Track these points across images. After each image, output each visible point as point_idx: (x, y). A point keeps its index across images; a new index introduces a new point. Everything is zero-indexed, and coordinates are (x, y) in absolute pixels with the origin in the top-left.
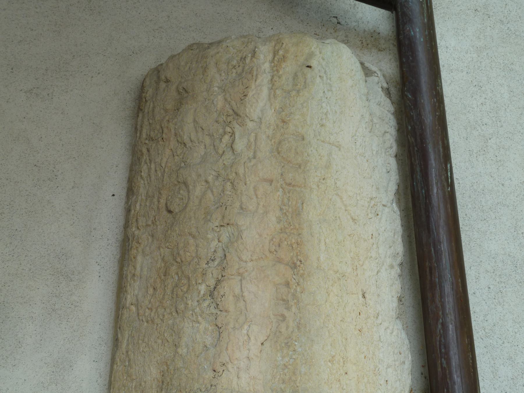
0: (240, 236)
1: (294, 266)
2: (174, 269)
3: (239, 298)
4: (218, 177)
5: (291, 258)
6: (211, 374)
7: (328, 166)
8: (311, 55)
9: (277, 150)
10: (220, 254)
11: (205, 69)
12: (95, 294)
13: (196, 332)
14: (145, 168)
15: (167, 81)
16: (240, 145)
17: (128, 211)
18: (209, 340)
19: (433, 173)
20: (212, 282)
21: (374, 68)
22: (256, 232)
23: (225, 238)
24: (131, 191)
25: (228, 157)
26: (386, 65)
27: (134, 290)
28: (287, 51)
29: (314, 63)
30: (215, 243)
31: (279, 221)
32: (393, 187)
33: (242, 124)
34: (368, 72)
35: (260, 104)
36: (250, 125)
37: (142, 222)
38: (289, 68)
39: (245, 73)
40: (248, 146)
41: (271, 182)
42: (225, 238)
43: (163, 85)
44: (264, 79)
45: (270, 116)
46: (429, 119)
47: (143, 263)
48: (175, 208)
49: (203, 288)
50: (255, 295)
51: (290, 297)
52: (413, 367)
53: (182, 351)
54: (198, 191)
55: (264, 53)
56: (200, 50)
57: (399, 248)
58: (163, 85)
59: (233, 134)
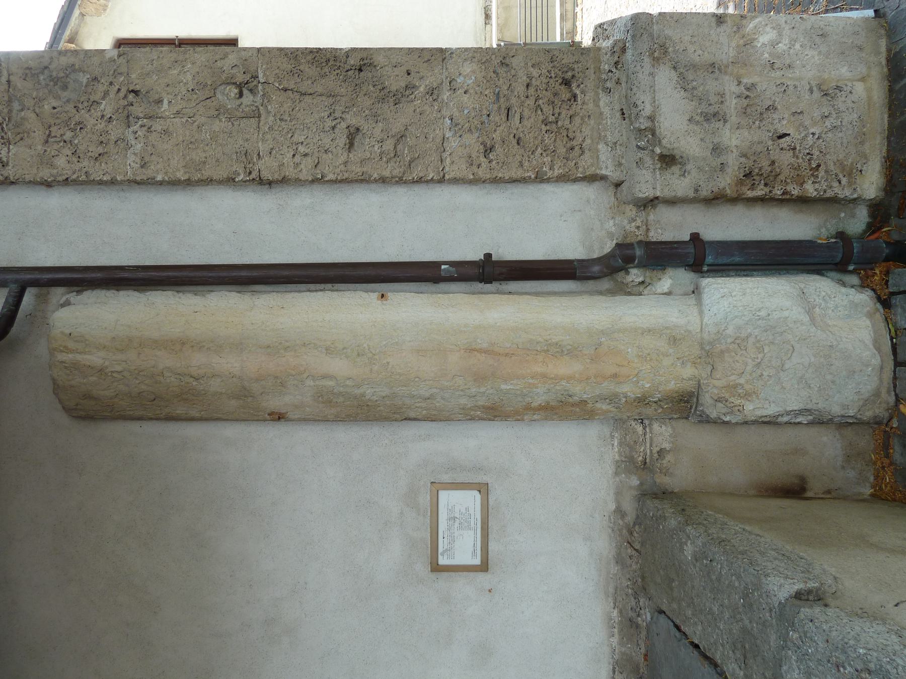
0: (169, 368)
1: (183, 344)
2: (184, 396)
3: (199, 367)
4: (136, 378)
5: (180, 344)
6: (234, 379)
7: (129, 327)
8: (62, 333)
9: (122, 351)
10: (177, 376)
11: (72, 386)
12: (192, 431)
13: (215, 385)
14: (128, 413)
15: (77, 405)
16: (119, 368)
17: (151, 419)
18: (219, 380)
19: (126, 275)
20: (192, 379)
21: (64, 299)
22: (165, 360)
23: (169, 374)
24: (140, 419)
25: (126, 374)
26: (58, 294)
27: (194, 413)
28: (61, 346)
29: (67, 332)
30: (172, 379)
31: (160, 350)
32: (136, 294)
33: (107, 367)
34: (67, 303)
35: (95, 359)
36: (107, 363)
37: (158, 412)
38: (71, 345)
39: (75, 366)
40: (119, 364)
41: (139, 354)
42: (169, 374)
43: (79, 407)
44: (79, 357)
45: (102, 354)
46: (99, 275)
47: (180, 411)
48: (152, 397)
49: (194, 383)
50: (198, 361)
51: (198, 345)
52: (190, 292)
53: (224, 391)
54: (143, 387)
55: (61, 357)
56: (57, 388)
57: (170, 293)
58: (79, 407)
59: (112, 372)
